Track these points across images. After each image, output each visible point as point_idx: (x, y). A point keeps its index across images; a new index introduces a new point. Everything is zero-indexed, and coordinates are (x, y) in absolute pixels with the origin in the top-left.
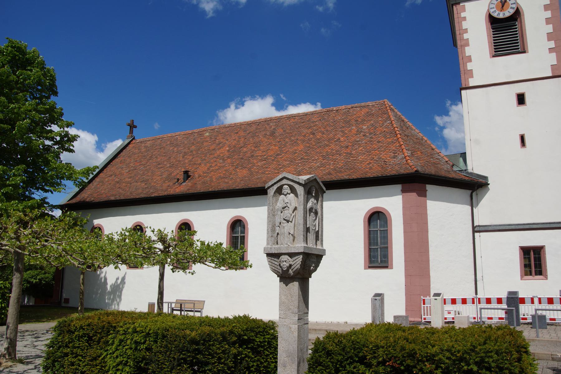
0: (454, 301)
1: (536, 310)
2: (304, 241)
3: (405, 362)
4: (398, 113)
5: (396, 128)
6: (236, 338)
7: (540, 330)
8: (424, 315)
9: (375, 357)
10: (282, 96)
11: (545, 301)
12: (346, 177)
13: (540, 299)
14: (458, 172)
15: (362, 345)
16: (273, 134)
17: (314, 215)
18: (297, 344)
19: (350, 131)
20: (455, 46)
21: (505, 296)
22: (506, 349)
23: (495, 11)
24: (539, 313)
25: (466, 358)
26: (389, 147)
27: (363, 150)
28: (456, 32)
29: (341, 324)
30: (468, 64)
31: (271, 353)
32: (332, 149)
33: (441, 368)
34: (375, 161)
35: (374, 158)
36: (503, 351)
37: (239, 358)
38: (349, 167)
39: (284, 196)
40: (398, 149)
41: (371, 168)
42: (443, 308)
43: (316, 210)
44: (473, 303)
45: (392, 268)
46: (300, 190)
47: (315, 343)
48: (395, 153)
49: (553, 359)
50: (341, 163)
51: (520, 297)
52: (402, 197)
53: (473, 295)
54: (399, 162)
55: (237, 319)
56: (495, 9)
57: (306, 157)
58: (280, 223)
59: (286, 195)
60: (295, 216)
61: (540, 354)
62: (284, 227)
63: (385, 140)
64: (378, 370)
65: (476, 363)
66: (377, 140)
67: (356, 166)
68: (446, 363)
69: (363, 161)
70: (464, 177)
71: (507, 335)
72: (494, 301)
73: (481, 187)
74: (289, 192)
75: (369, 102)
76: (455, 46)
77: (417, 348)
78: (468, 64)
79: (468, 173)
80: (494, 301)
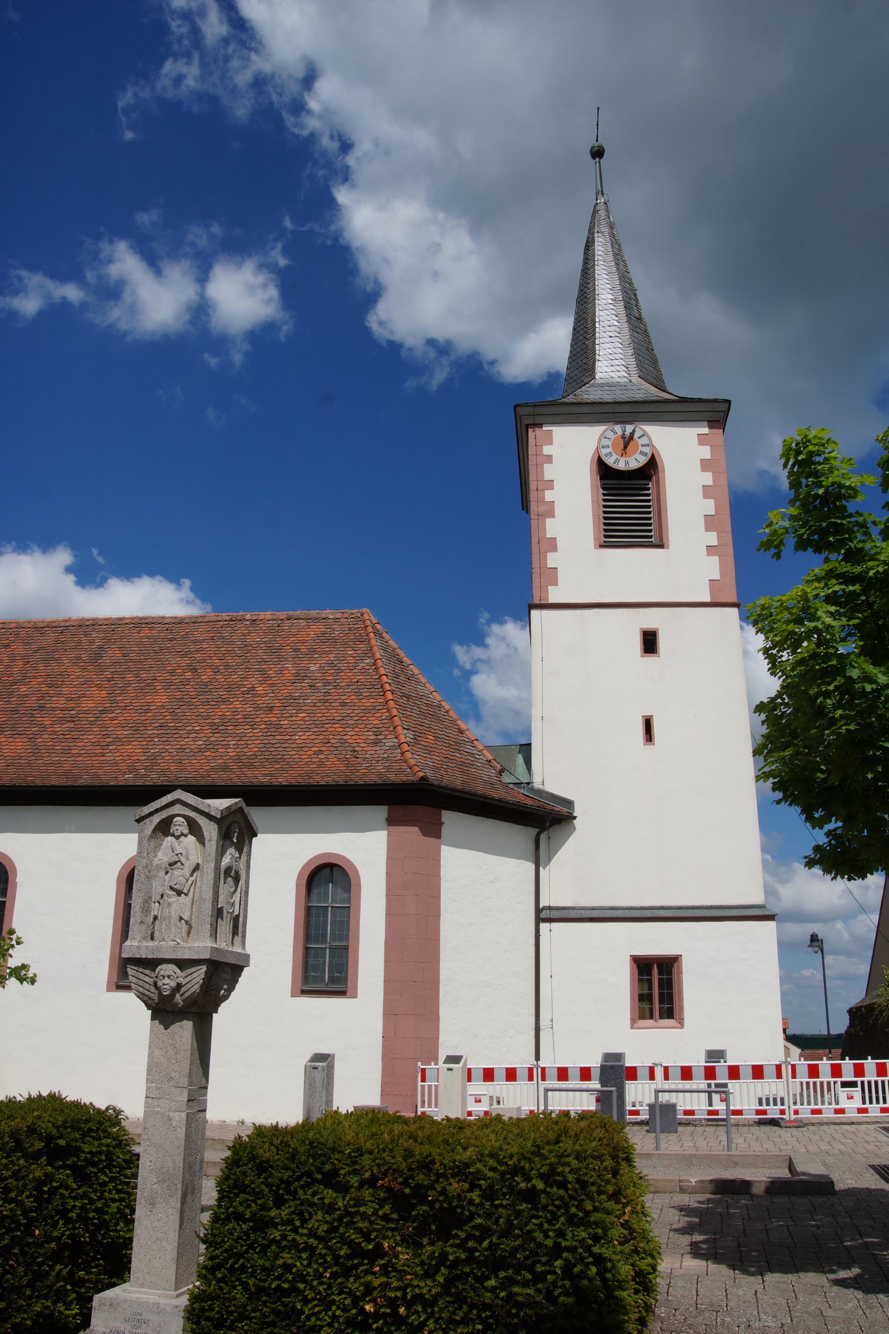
0: (489, 1075)
1: (657, 1092)
2: (211, 936)
3: (414, 1180)
4: (391, 642)
5: (384, 677)
6: (43, 1144)
7: (663, 1136)
8: (423, 1106)
9: (355, 1172)
10: (95, 552)
11: (675, 1073)
12: (265, 780)
13: (666, 1069)
14: (511, 786)
15: (329, 1148)
16: (96, 657)
17: (232, 883)
18: (182, 1154)
19: (281, 672)
20: (525, 509)
21: (597, 1063)
22: (594, 1151)
23: (610, 454)
24: (664, 1098)
25: (523, 1168)
26: (365, 718)
27: (307, 719)
28: (529, 484)
29: (229, 1126)
30: (549, 555)
31: (112, 1179)
32: (234, 710)
33: (480, 1186)
34: (332, 749)
35: (331, 741)
36: (588, 1153)
37: (46, 1189)
38: (271, 757)
39: (174, 839)
40: (385, 725)
41: (321, 764)
42: (464, 1090)
43: (237, 873)
44: (531, 1078)
45: (355, 996)
46: (210, 830)
47: (234, 1146)
48: (378, 733)
49: (682, 1190)
50: (254, 746)
51: (627, 1065)
52: (388, 835)
53: (530, 1061)
54: (386, 756)
55: (36, 1103)
56: (610, 450)
57: (173, 724)
58: (162, 896)
59: (178, 838)
60: (194, 883)
61: (658, 1180)
62: (169, 904)
63: (357, 701)
64: (362, 1196)
65: (542, 1176)
66: (340, 701)
67: (288, 757)
68: (489, 1178)
69: (304, 745)
70: (523, 798)
71: (597, 1127)
72: (574, 1074)
73: (559, 823)
74: (186, 831)
75: (328, 611)
76: (525, 509)
77: (435, 1151)
78: (549, 555)
79: (533, 790)
80: (574, 1074)
